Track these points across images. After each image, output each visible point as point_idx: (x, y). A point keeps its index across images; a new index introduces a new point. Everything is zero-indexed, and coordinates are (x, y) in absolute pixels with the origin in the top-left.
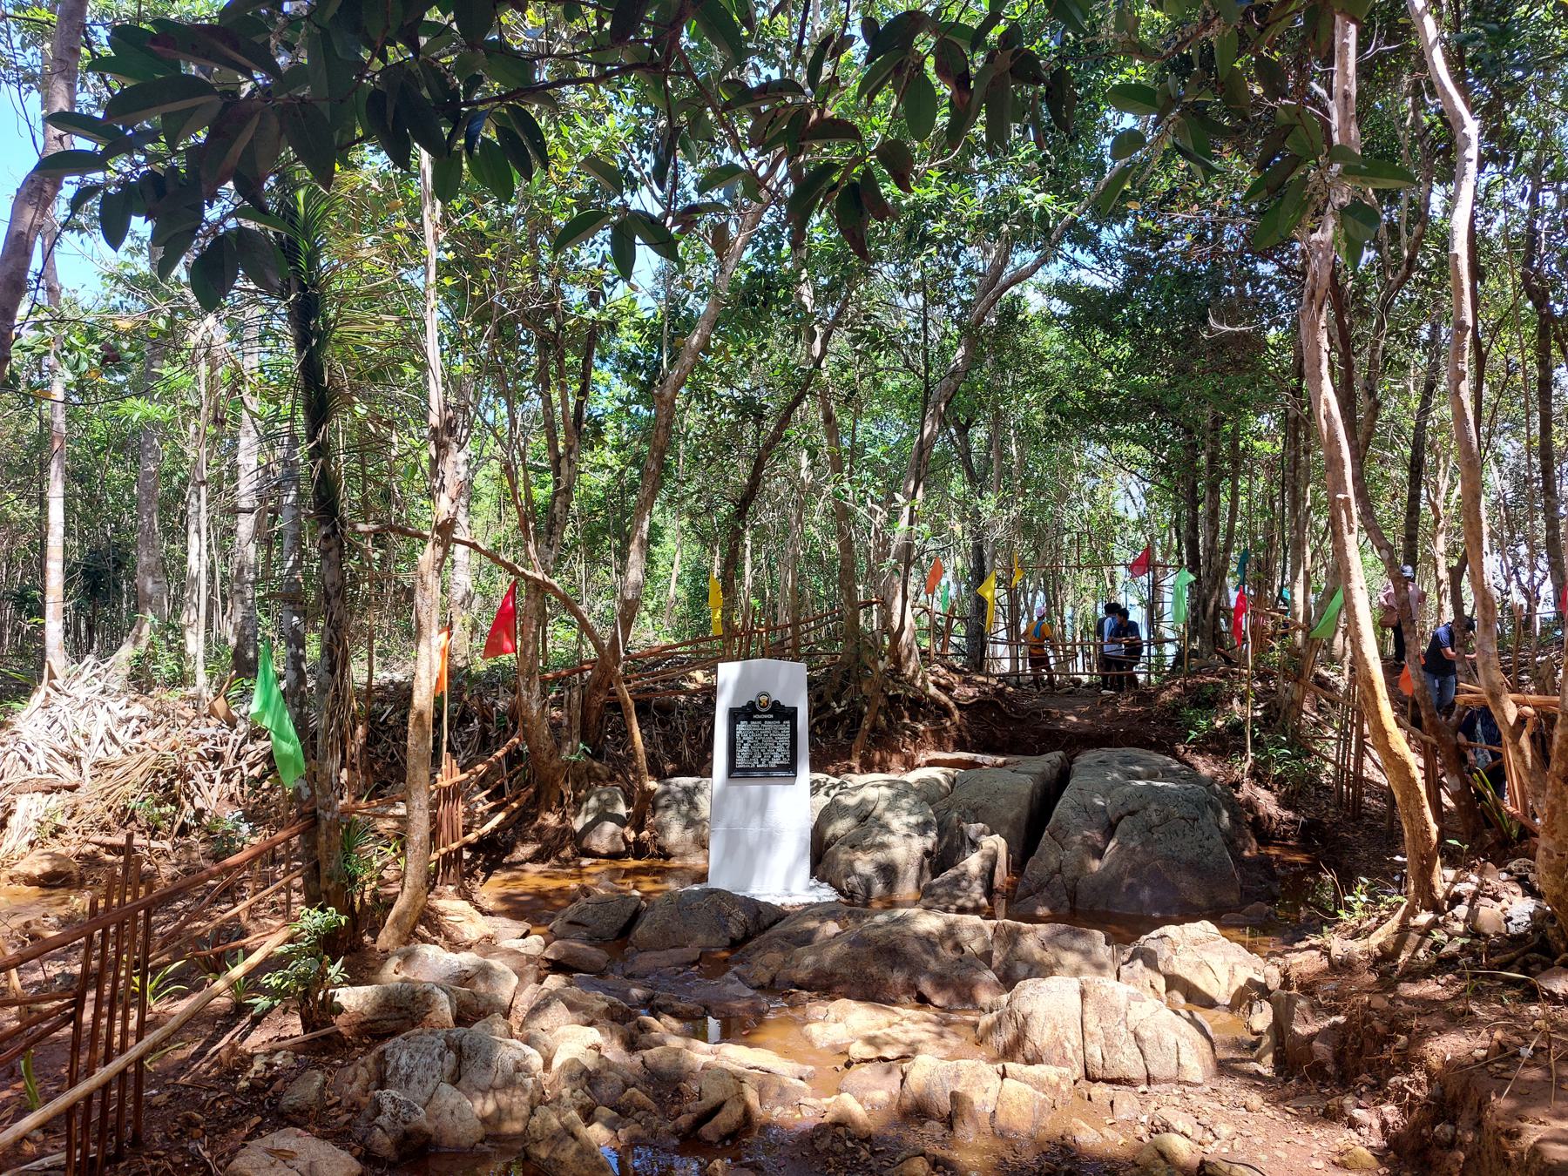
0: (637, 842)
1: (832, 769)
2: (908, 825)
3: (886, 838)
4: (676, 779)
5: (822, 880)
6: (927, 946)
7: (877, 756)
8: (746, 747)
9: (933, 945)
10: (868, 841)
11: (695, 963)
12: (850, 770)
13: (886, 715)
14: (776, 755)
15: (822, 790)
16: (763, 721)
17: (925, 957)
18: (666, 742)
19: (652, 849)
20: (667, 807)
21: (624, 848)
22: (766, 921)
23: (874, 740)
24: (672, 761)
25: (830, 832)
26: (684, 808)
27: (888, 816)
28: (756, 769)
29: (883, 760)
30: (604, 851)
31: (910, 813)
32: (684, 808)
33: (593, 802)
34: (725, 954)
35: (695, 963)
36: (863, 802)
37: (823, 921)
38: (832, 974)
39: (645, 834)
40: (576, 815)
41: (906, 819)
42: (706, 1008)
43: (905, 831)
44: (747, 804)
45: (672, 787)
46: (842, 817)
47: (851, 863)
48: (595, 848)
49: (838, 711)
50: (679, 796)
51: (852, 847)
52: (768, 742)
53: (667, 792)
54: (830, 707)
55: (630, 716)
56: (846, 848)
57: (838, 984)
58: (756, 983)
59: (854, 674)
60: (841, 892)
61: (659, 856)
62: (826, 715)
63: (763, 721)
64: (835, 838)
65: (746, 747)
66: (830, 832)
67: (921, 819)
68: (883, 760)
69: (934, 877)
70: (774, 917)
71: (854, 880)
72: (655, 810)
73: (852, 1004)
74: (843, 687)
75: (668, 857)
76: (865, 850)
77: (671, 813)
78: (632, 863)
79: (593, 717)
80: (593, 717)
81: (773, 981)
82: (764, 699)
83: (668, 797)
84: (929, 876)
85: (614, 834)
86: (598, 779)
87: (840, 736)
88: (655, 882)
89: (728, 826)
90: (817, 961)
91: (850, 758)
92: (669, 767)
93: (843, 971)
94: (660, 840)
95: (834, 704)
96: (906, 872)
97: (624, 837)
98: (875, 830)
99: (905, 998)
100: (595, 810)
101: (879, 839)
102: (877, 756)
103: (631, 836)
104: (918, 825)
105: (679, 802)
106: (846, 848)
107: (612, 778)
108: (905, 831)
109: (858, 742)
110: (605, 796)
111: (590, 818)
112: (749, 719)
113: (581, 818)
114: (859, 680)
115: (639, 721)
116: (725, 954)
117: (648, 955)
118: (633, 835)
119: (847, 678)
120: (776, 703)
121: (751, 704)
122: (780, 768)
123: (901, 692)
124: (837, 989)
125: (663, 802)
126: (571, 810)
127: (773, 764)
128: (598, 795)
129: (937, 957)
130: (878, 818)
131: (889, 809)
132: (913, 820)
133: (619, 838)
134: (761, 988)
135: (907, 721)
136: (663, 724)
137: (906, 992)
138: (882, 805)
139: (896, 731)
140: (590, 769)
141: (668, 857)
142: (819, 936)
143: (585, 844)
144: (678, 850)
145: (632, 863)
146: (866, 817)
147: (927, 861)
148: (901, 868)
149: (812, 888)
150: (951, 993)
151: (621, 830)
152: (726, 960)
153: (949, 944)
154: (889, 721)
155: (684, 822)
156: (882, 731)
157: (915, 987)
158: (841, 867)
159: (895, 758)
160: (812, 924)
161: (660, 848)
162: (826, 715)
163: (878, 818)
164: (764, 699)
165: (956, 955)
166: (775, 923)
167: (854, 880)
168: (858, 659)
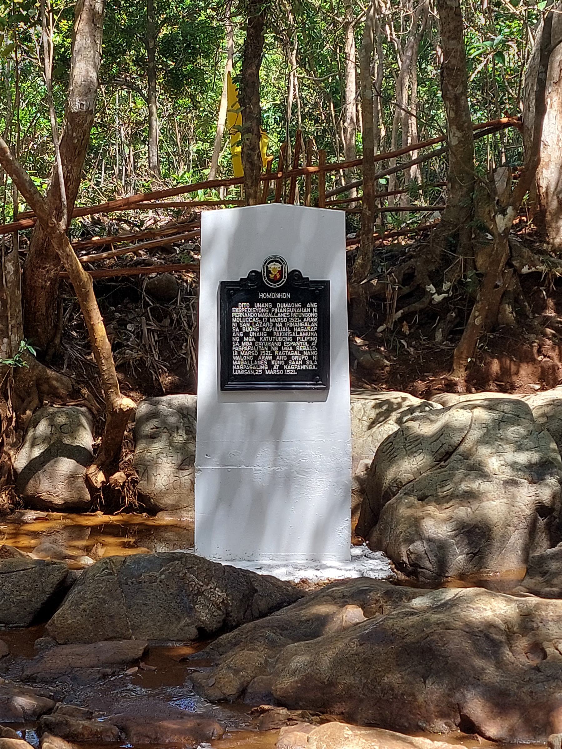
0: (106, 487)
1: (421, 385)
2: (514, 466)
3: (476, 485)
4: (169, 397)
5: (374, 547)
6: (485, 646)
7: (495, 366)
8: (248, 343)
9: (496, 645)
10: (448, 488)
11: (134, 662)
12: (450, 388)
13: (516, 303)
14: (295, 356)
15: (394, 416)
16: (274, 302)
17: (478, 662)
18: (163, 343)
19: (129, 498)
20: (153, 437)
21: (88, 497)
22: (263, 605)
23: (492, 344)
24: (171, 371)
25: (390, 475)
26: (180, 438)
27: (484, 451)
28: (264, 377)
29: (505, 372)
30: (58, 501)
31: (519, 448)
32: (180, 438)
33: (43, 427)
34: (187, 651)
35: (134, 662)
36: (446, 429)
37: (344, 605)
38: (332, 684)
39: (119, 476)
40: (18, 446)
41: (511, 456)
42: (123, 729)
43: (508, 474)
44: (252, 424)
45: (163, 408)
46: (411, 453)
47: (416, 522)
48: (45, 496)
49: (438, 298)
50: (172, 420)
51: (422, 499)
52: (282, 334)
53: (153, 415)
54: (424, 293)
55: (86, 297)
56: (413, 499)
57: (341, 699)
58: (216, 694)
59: (464, 240)
60: (399, 565)
61: (141, 510)
62: (418, 306)
63: (274, 302)
64: (398, 484)
65: (248, 343)
66: (390, 475)
67: (535, 457)
68: (505, 372)
69: (553, 546)
70: (277, 597)
71: (419, 546)
72: (135, 440)
73: (347, 730)
74: (446, 261)
75: (153, 510)
76: (440, 501)
77: (157, 446)
78: (100, 518)
79: (42, 300)
80: (42, 300)
81: (243, 692)
82: (275, 267)
83: (154, 423)
84: (545, 543)
85: (72, 477)
86: (55, 396)
87: (439, 336)
88: (125, 545)
89: (224, 461)
90: (311, 663)
91: (450, 370)
92: (166, 379)
93: (349, 680)
94: (142, 486)
95: (431, 288)
96: (505, 538)
97: (87, 480)
98: (460, 474)
99: (440, 725)
100: (46, 439)
101: (464, 487)
102: (495, 366)
103: (99, 478)
104: (530, 467)
105: (172, 430)
106: (413, 499)
107: (75, 394)
108: (508, 474)
109: (464, 345)
110: (61, 419)
111: (37, 452)
112: (252, 300)
113: (25, 451)
114: (472, 250)
115: (103, 312)
116: (187, 651)
117: (67, 649)
118: (101, 477)
119: (453, 248)
120: (295, 275)
121: (255, 276)
122: (301, 375)
123: (541, 268)
124: (338, 708)
125: (147, 429)
126: (12, 439)
127: (290, 370)
128: (51, 418)
129: (500, 664)
130: (467, 456)
131: (485, 440)
132: (523, 458)
133: (80, 482)
134: (223, 702)
135: (550, 313)
136: (159, 316)
137: (442, 715)
138: (475, 434)
139: (531, 329)
140: (41, 381)
141: (153, 510)
142: (332, 628)
143: (30, 489)
144: (168, 500)
145: (100, 518)
146: (448, 454)
147: (542, 522)
148: (497, 532)
149: (355, 558)
150: (515, 719)
151: (83, 470)
152: (184, 660)
153: (522, 643)
154: (521, 314)
155: (177, 458)
156: (507, 330)
157: (458, 708)
158: (401, 528)
159: (525, 370)
160: (323, 609)
161: (142, 497)
162: (418, 306)
163: (467, 456)
164: (275, 267)
165: (534, 661)
166: (279, 607)
167: (419, 546)
168: (471, 217)
